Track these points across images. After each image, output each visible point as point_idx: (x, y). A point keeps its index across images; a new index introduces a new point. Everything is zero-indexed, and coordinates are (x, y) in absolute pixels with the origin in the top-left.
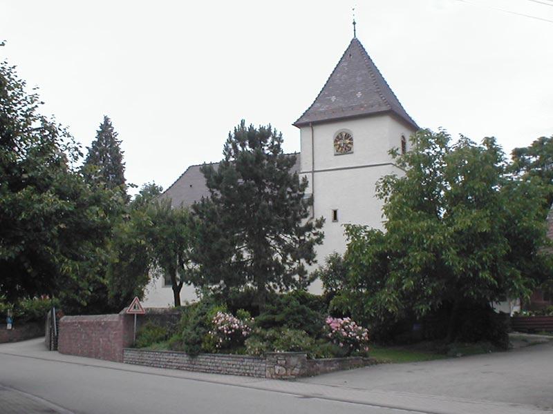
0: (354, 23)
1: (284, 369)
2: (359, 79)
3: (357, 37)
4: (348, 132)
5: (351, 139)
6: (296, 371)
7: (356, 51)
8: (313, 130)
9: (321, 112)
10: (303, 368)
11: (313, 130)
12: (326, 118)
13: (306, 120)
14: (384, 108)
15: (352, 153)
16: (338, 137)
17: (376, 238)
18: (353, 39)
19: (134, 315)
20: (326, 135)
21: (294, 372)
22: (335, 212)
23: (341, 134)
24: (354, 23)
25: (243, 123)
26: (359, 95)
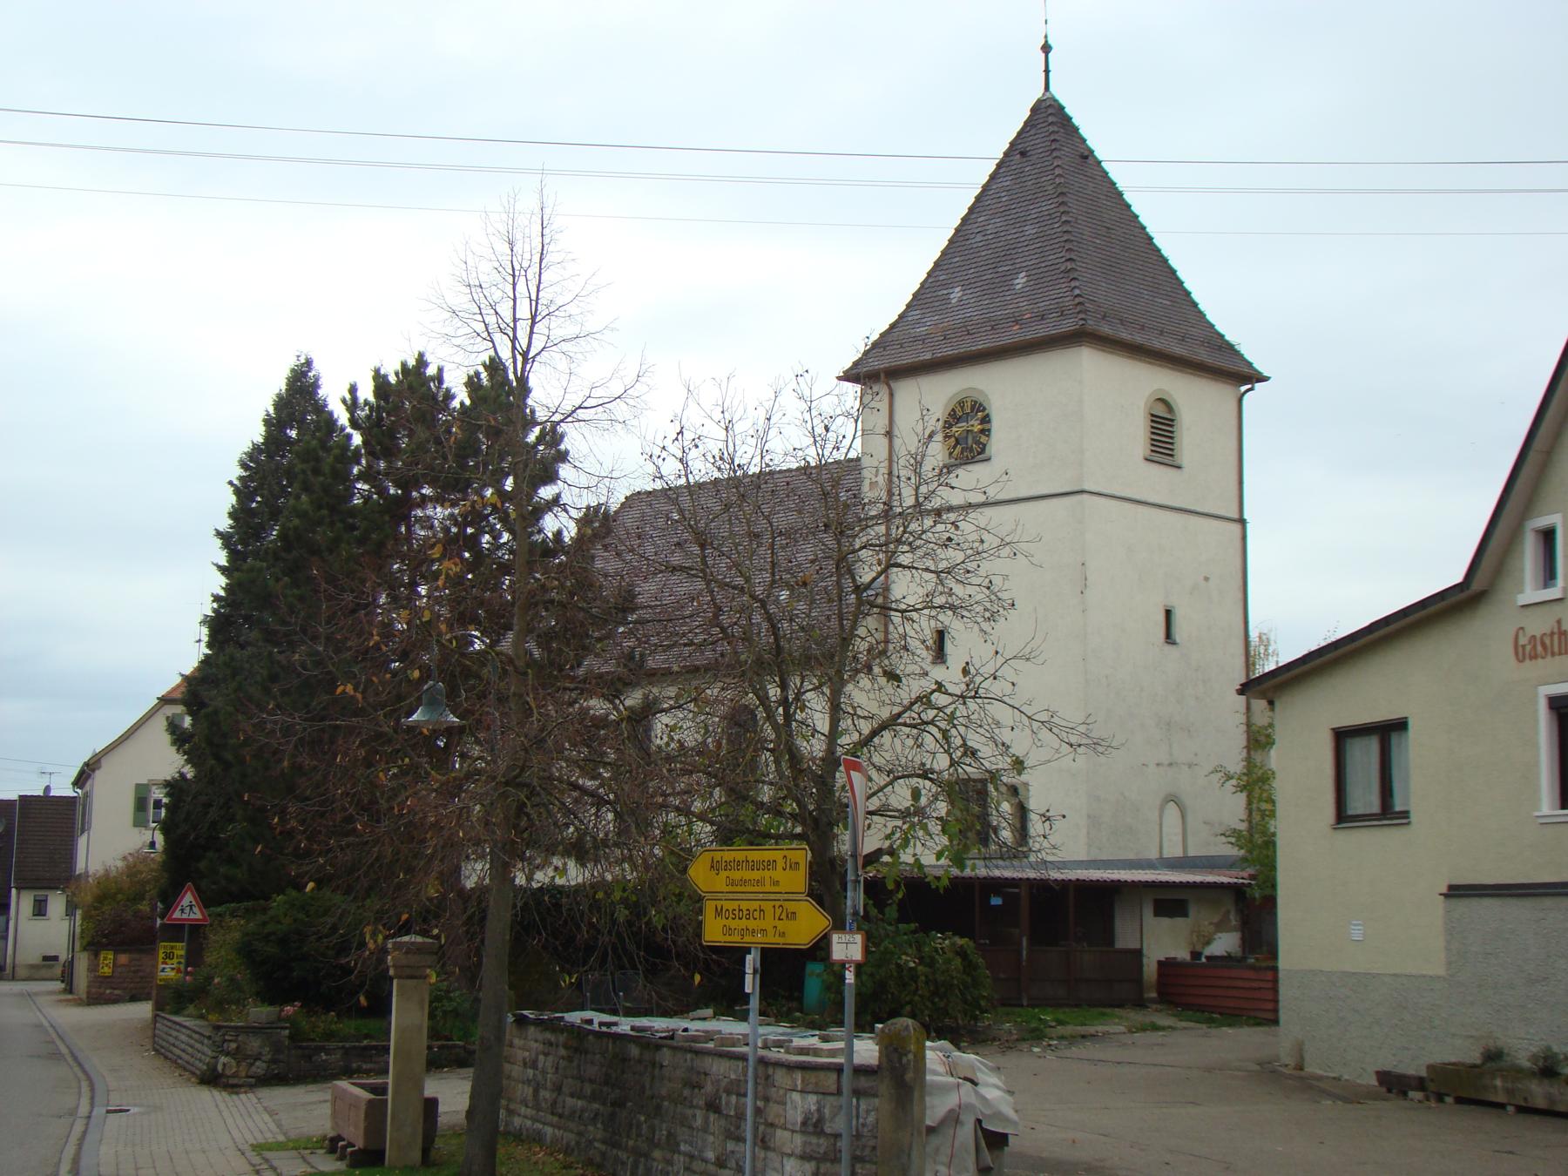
0: (1046, 48)
1: (234, 1063)
2: (1030, 230)
3: (1055, 90)
4: (981, 399)
5: (986, 420)
6: (260, 1068)
7: (1049, 135)
8: (891, 395)
9: (916, 339)
10: (274, 1061)
11: (891, 395)
12: (928, 356)
13: (875, 364)
14: (1068, 325)
15: (988, 459)
16: (952, 414)
17: (175, 787)
18: (1039, 102)
19: (740, 953)
20: (924, 402)
21: (254, 1069)
22: (1168, 613)
23: (961, 403)
24: (1046, 48)
25: (231, 483)
26: (1021, 280)
